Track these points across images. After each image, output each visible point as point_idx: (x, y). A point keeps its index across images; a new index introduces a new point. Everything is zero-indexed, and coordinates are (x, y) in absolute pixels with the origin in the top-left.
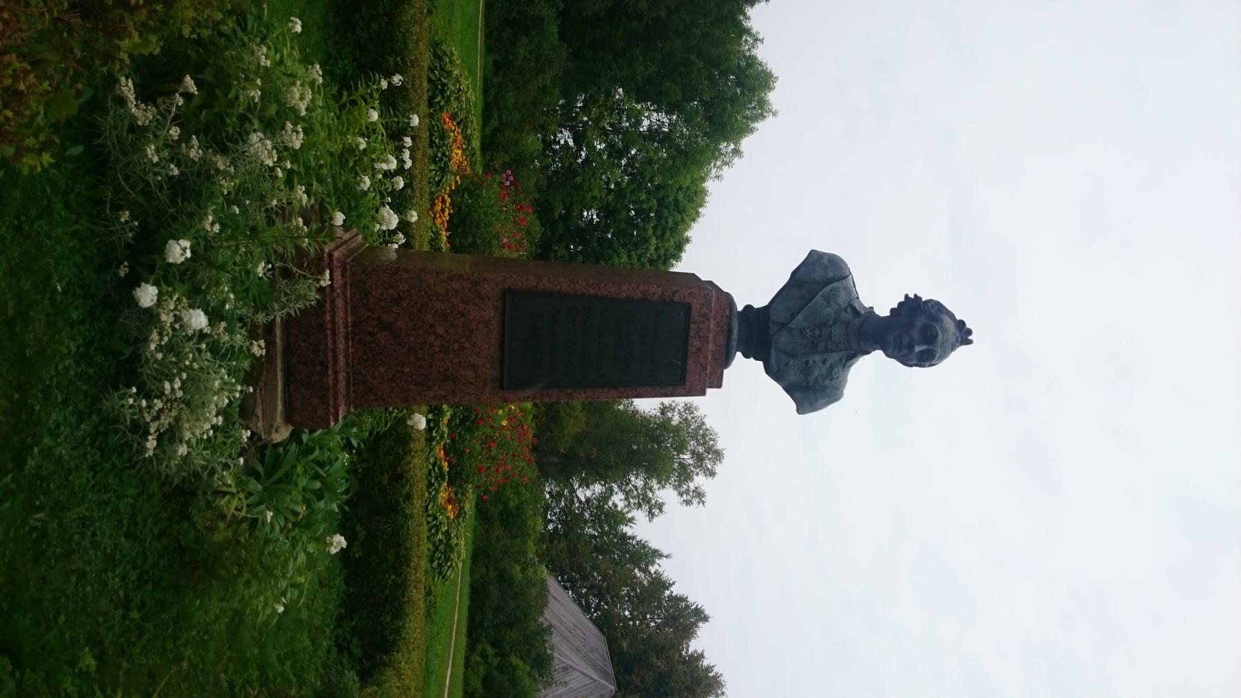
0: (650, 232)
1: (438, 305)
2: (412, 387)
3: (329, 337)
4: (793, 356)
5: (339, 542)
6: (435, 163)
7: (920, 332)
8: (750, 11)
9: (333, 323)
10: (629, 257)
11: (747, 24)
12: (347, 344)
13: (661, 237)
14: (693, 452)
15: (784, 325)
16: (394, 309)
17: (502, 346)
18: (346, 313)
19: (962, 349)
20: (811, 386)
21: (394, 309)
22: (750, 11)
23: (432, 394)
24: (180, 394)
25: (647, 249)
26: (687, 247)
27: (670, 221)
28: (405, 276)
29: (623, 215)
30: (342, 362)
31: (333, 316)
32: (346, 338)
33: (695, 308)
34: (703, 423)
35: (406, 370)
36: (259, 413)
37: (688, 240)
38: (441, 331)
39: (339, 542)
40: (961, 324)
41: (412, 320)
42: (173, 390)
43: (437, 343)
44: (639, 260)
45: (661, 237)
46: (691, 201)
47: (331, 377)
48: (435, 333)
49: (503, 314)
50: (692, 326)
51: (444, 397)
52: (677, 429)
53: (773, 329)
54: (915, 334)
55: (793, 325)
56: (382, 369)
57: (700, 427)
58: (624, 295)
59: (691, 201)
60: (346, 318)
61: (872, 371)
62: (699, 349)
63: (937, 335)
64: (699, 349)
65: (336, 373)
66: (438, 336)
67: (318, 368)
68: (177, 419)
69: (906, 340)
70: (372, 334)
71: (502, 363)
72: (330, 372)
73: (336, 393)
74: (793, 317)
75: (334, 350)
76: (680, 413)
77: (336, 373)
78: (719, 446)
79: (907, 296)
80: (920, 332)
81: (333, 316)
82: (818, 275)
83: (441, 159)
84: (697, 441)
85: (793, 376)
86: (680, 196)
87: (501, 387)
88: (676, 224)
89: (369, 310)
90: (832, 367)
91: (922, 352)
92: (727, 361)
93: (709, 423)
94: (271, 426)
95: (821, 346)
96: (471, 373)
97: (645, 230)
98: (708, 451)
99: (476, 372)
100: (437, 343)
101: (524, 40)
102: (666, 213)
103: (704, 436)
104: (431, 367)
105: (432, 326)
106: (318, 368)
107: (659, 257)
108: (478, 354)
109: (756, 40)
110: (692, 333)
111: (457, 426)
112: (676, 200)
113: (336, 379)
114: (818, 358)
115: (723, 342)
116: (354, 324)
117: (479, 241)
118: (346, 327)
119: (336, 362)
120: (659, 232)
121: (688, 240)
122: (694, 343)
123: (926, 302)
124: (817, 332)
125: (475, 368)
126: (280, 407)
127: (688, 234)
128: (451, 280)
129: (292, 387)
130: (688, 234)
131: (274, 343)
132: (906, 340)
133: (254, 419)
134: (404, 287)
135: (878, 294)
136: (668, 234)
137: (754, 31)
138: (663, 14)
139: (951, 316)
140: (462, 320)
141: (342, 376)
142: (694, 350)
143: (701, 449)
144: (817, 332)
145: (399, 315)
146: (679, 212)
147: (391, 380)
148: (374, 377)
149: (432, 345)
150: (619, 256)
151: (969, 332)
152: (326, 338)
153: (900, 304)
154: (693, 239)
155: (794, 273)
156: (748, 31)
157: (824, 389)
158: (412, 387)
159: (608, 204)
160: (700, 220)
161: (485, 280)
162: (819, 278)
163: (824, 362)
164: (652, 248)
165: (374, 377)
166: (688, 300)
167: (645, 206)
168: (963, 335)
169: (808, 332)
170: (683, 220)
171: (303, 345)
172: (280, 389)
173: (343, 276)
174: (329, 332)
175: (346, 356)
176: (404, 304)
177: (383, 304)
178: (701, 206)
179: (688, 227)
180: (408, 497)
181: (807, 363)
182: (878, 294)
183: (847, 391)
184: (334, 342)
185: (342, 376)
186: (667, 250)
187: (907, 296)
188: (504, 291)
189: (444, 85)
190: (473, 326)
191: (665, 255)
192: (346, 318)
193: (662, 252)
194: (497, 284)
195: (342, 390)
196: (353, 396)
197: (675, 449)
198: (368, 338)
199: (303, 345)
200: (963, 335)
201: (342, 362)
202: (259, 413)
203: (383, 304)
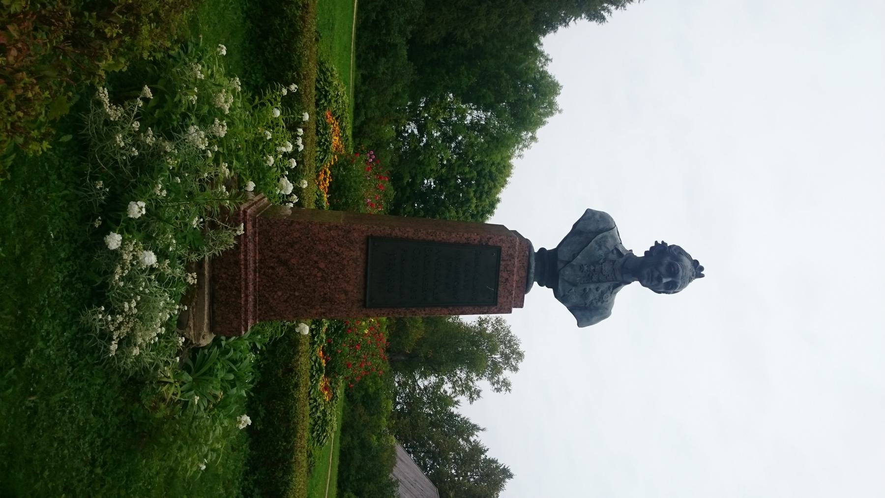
0: (472, 194)
1: (320, 247)
2: (301, 306)
3: (243, 271)
4: (574, 284)
5: (246, 420)
6: (320, 146)
7: (666, 268)
8: (542, 39)
9: (246, 260)
10: (457, 212)
12: (255, 275)
13: (480, 198)
14: (502, 354)
15: (568, 263)
16: (289, 250)
17: (365, 277)
19: (697, 281)
20: (588, 307)
21: (289, 250)
22: (542, 39)
23: (315, 312)
24: (135, 311)
25: (470, 207)
26: (498, 205)
28: (297, 226)
29: (452, 183)
30: (251, 288)
31: (246, 256)
32: (255, 271)
33: (504, 249)
34: (509, 332)
36: (192, 325)
37: (498, 200)
38: (322, 265)
39: (246, 420)
40: (696, 263)
41: (302, 258)
43: (319, 275)
44: (464, 214)
45: (480, 198)
47: (243, 299)
48: (318, 267)
49: (367, 254)
51: (324, 313)
52: (490, 336)
53: (560, 265)
54: (663, 269)
55: (574, 262)
56: (280, 293)
57: (506, 335)
58: (453, 240)
60: (255, 257)
61: (632, 297)
65: (247, 296)
66: (320, 269)
67: (234, 293)
69: (656, 274)
70: (273, 268)
71: (365, 288)
73: (246, 311)
74: (574, 257)
75: (246, 280)
76: (493, 325)
77: (247, 296)
78: (521, 348)
79: (656, 242)
80: (666, 268)
81: (246, 256)
82: (592, 227)
83: (324, 144)
85: (575, 299)
87: (364, 306)
88: (490, 189)
89: (272, 251)
90: (603, 293)
91: (668, 283)
92: (527, 288)
93: (514, 332)
94: (200, 334)
95: (595, 278)
96: (343, 296)
97: (468, 193)
98: (513, 352)
99: (346, 295)
101: (384, 60)
102: (483, 181)
103: (509, 341)
104: (314, 291)
105: (316, 262)
106: (234, 293)
107: (478, 212)
108: (348, 282)
109: (547, 60)
110: (502, 268)
111: (332, 334)
112: (490, 172)
113: (246, 300)
114: (592, 286)
115: (524, 274)
116: (261, 261)
117: (350, 201)
118: (255, 263)
119: (247, 288)
120: (478, 195)
121: (498, 200)
122: (504, 275)
124: (591, 268)
125: (346, 292)
126: (206, 321)
127: (499, 196)
128: (330, 230)
129: (215, 306)
130: (499, 196)
131: (204, 275)
132: (656, 274)
133: (187, 329)
134: (296, 234)
135: (636, 241)
136: (484, 196)
137: (545, 53)
138: (481, 41)
140: (338, 258)
141: (251, 299)
142: (503, 280)
143: (508, 351)
144: (591, 268)
145: (292, 254)
146: (493, 181)
147: (286, 301)
148: (274, 299)
149: (316, 276)
150: (449, 212)
151: (702, 269)
153: (652, 248)
154: (502, 200)
155: (575, 226)
156: (541, 54)
158: (301, 306)
160: (507, 186)
163: (597, 289)
164: (473, 206)
165: (274, 299)
167: (468, 176)
168: (698, 271)
170: (495, 186)
171: (224, 276)
172: (206, 308)
173: (253, 227)
174: (242, 267)
175: (254, 284)
176: (296, 247)
178: (508, 176)
180: (296, 386)
181: (585, 290)
183: (614, 310)
184: (246, 274)
185: (251, 299)
187: (656, 242)
188: (368, 237)
189: (326, 91)
190: (345, 262)
193: (480, 209)
194: (363, 233)
198: (270, 271)
199: (224, 276)
200: (698, 271)
201: (251, 288)
202: (192, 325)
203: (281, 246)
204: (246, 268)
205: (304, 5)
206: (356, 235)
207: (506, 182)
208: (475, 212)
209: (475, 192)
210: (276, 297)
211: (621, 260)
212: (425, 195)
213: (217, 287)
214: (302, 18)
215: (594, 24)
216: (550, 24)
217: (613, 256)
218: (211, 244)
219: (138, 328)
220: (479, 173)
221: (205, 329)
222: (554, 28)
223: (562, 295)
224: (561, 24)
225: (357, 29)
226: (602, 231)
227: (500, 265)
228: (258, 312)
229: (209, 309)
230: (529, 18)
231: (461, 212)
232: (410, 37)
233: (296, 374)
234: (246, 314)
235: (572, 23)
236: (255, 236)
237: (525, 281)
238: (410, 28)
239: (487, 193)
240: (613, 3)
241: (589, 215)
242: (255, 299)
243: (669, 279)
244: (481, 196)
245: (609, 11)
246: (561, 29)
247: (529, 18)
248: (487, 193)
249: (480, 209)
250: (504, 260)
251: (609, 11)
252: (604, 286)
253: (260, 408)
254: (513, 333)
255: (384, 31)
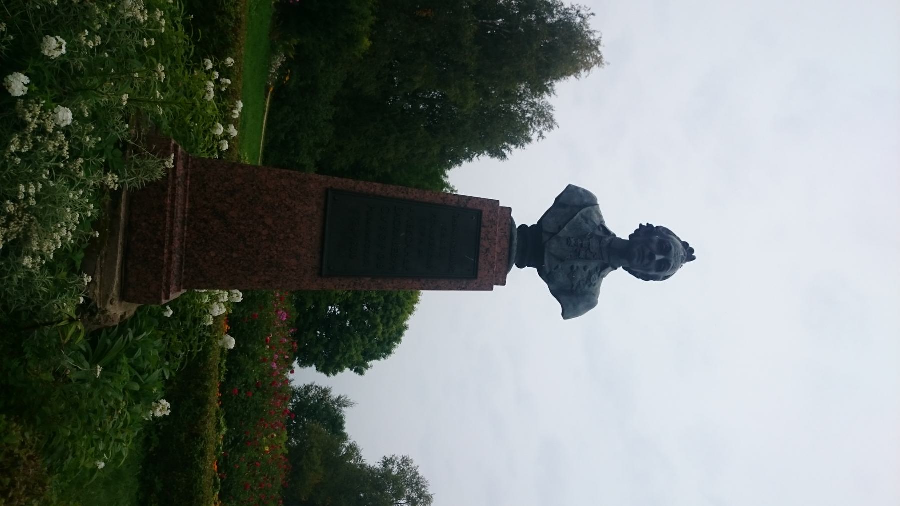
0: (379, 320)
2: (239, 271)
3: (168, 219)
4: (562, 260)
5: (163, 408)
7: (655, 253)
8: (448, 172)
9: (173, 207)
10: (362, 338)
11: (445, 180)
12: (183, 228)
13: (387, 325)
14: (409, 498)
15: (553, 235)
18: (185, 199)
19: (687, 265)
20: (575, 296)
22: (448, 172)
24: (33, 202)
25: (376, 333)
26: (406, 332)
27: (394, 312)
28: (240, 171)
29: (359, 308)
30: (177, 244)
31: (173, 201)
33: (485, 213)
34: (417, 473)
35: (235, 255)
37: (406, 327)
38: (269, 221)
39: (163, 408)
40: (686, 244)
42: (27, 195)
43: (265, 232)
44: (370, 341)
45: (387, 325)
46: (409, 298)
47: (166, 256)
49: (325, 210)
50: (483, 229)
51: (269, 282)
52: (396, 479)
53: (546, 237)
54: (654, 246)
55: (561, 234)
57: (414, 476)
58: (427, 200)
59: (409, 298)
60: (184, 205)
61: (617, 283)
62: (488, 250)
63: (671, 248)
64: (488, 250)
65: (171, 253)
67: (156, 246)
68: (27, 229)
69: (648, 252)
71: (322, 253)
72: (166, 251)
73: (169, 272)
74: (560, 228)
75: (171, 231)
76: (399, 465)
77: (171, 253)
78: (430, 491)
79: (641, 225)
80: (655, 253)
81: (173, 201)
82: (576, 201)
84: (412, 487)
85: (562, 278)
86: (401, 294)
87: (320, 275)
88: (398, 314)
90: (590, 274)
91: (660, 261)
92: (509, 269)
93: (421, 472)
94: (107, 296)
95: (583, 253)
97: (375, 319)
98: (420, 496)
100: (265, 232)
102: (390, 306)
103: (417, 483)
105: (261, 217)
107: (385, 339)
110: (483, 235)
111: (230, 446)
112: (398, 297)
113: (170, 258)
114: (580, 264)
117: (257, 295)
118: (184, 213)
119: (171, 242)
120: (385, 321)
121: (406, 327)
122: (484, 243)
123: (657, 227)
124: (576, 251)
126: (117, 279)
127: (407, 322)
130: (407, 322)
131: (118, 217)
132: (648, 252)
135: (621, 224)
136: (392, 322)
137: (451, 185)
138: (389, 170)
139: (679, 239)
141: (176, 257)
143: (415, 495)
144: (576, 251)
146: (400, 306)
150: (354, 338)
151: (692, 250)
152: (165, 219)
153: (637, 231)
154: (410, 327)
155: (557, 199)
157: (584, 294)
158: (239, 271)
159: (348, 299)
160: (415, 312)
161: (310, 179)
162: (574, 205)
163: (585, 268)
164: (380, 333)
166: (479, 208)
167: (375, 301)
168: (689, 254)
169: (573, 241)
170: (403, 312)
171: (144, 224)
172: (118, 262)
173: (185, 167)
174: (168, 214)
177: (218, 194)
178: (416, 302)
179: (406, 318)
180: (203, 453)
181: (572, 267)
182: (621, 224)
183: (600, 299)
184: (172, 224)
185: (176, 257)
186: (391, 334)
187: (641, 225)
191: (389, 338)
192: (184, 205)
193: (387, 335)
195: (175, 271)
196: (184, 277)
197: (395, 495)
200: (689, 254)
201: (177, 244)
203: (218, 194)
204: (172, 216)
205: (237, 19)
206: (312, 186)
207: (413, 308)
208: (382, 339)
209: (382, 317)
210: (207, 258)
211: (608, 239)
212: (329, 322)
213: (134, 239)
214: (234, 31)
215: (496, 160)
216: (457, 160)
217: (600, 233)
218: (133, 170)
219: (34, 228)
220: (386, 298)
221: (115, 291)
222: (459, 163)
223: (548, 270)
224: (465, 159)
225: (265, 148)
226: (586, 206)
227: (480, 231)
228: (184, 277)
229: (122, 262)
230: (436, 150)
231: (367, 339)
232: (319, 159)
233: (202, 439)
234: (169, 277)
235: (475, 158)
236: (186, 179)
237: (507, 253)
238: (320, 150)
239: (394, 318)
240: (513, 143)
241: (571, 191)
242: (181, 258)
243: (662, 257)
244: (388, 322)
245: (509, 149)
246: (465, 163)
247: (436, 150)
248: (394, 318)
249: (387, 335)
250: (484, 227)
251: (509, 149)
252: (593, 265)
253: (156, 480)
254: (421, 474)
255: (293, 152)
